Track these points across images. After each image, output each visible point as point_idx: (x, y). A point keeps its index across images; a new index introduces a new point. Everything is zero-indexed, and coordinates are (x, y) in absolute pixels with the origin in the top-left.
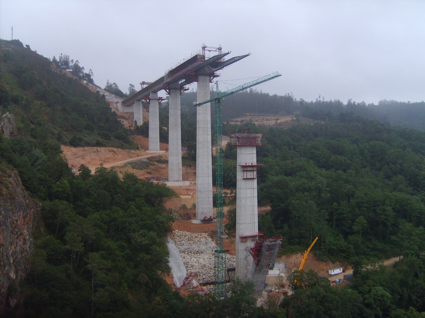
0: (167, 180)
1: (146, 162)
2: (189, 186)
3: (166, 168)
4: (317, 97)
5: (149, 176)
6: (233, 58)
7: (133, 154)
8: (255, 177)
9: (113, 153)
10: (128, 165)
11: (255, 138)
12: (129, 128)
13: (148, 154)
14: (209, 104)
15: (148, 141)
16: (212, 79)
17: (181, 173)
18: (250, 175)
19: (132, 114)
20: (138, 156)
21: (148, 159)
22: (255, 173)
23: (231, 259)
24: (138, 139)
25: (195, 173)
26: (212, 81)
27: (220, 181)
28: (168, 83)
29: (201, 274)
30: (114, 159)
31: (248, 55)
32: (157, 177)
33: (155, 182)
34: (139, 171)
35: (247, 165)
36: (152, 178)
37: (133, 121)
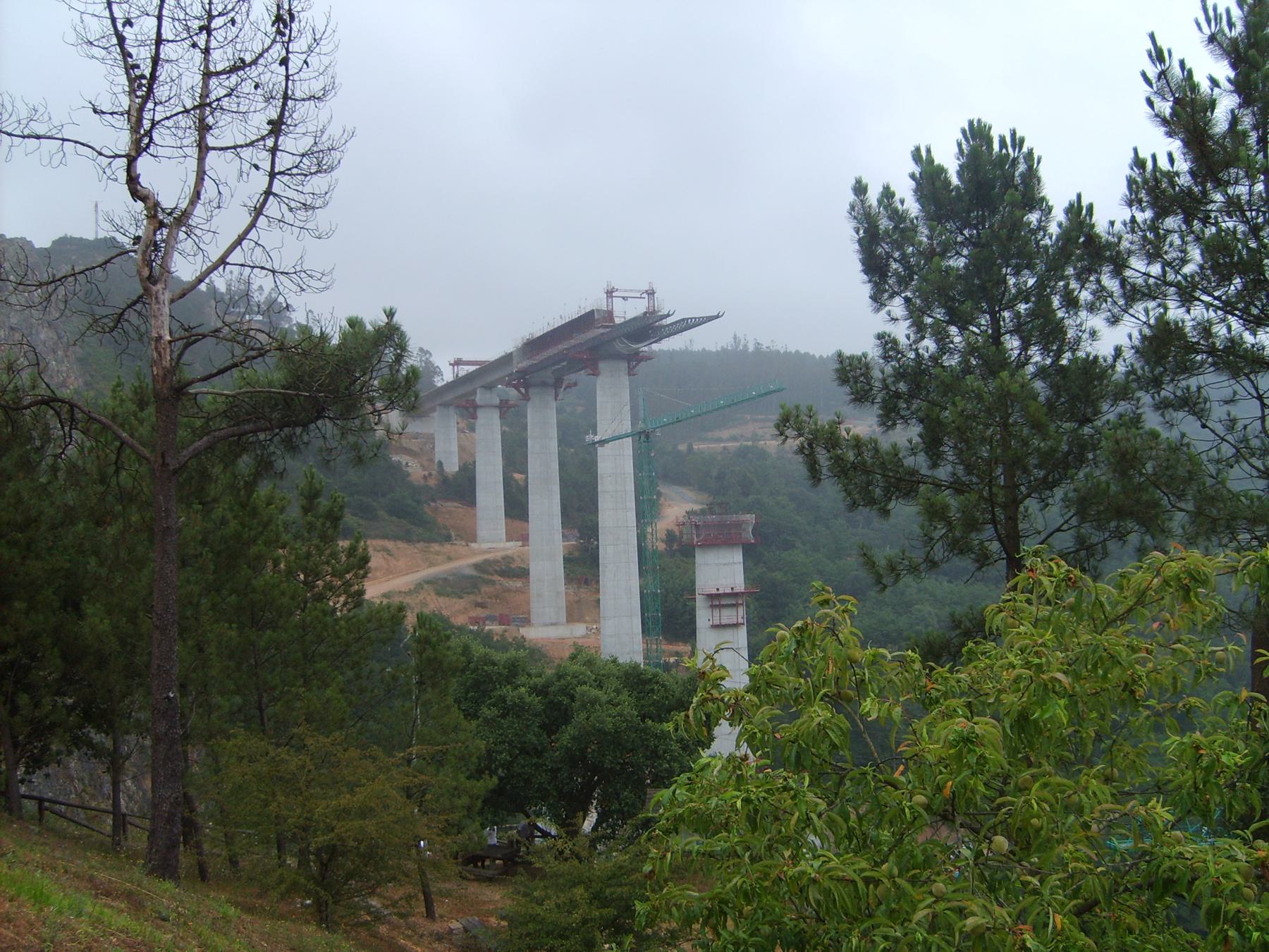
0: (527, 621)
1: (471, 577)
2: (584, 637)
3: (524, 591)
5: (480, 612)
6: (683, 320)
7: (437, 553)
8: (740, 621)
9: (385, 554)
10: (426, 586)
11: (739, 525)
12: (422, 482)
13: (474, 553)
14: (630, 439)
15: (475, 515)
16: (634, 367)
17: (563, 603)
18: (728, 616)
19: (430, 439)
20: (450, 559)
21: (476, 566)
22: (741, 611)
24: (449, 510)
25: (598, 601)
28: (523, 373)
30: (387, 570)
31: (717, 317)
32: (501, 615)
33: (496, 628)
34: (454, 600)
35: (721, 591)
36: (488, 618)
37: (432, 460)
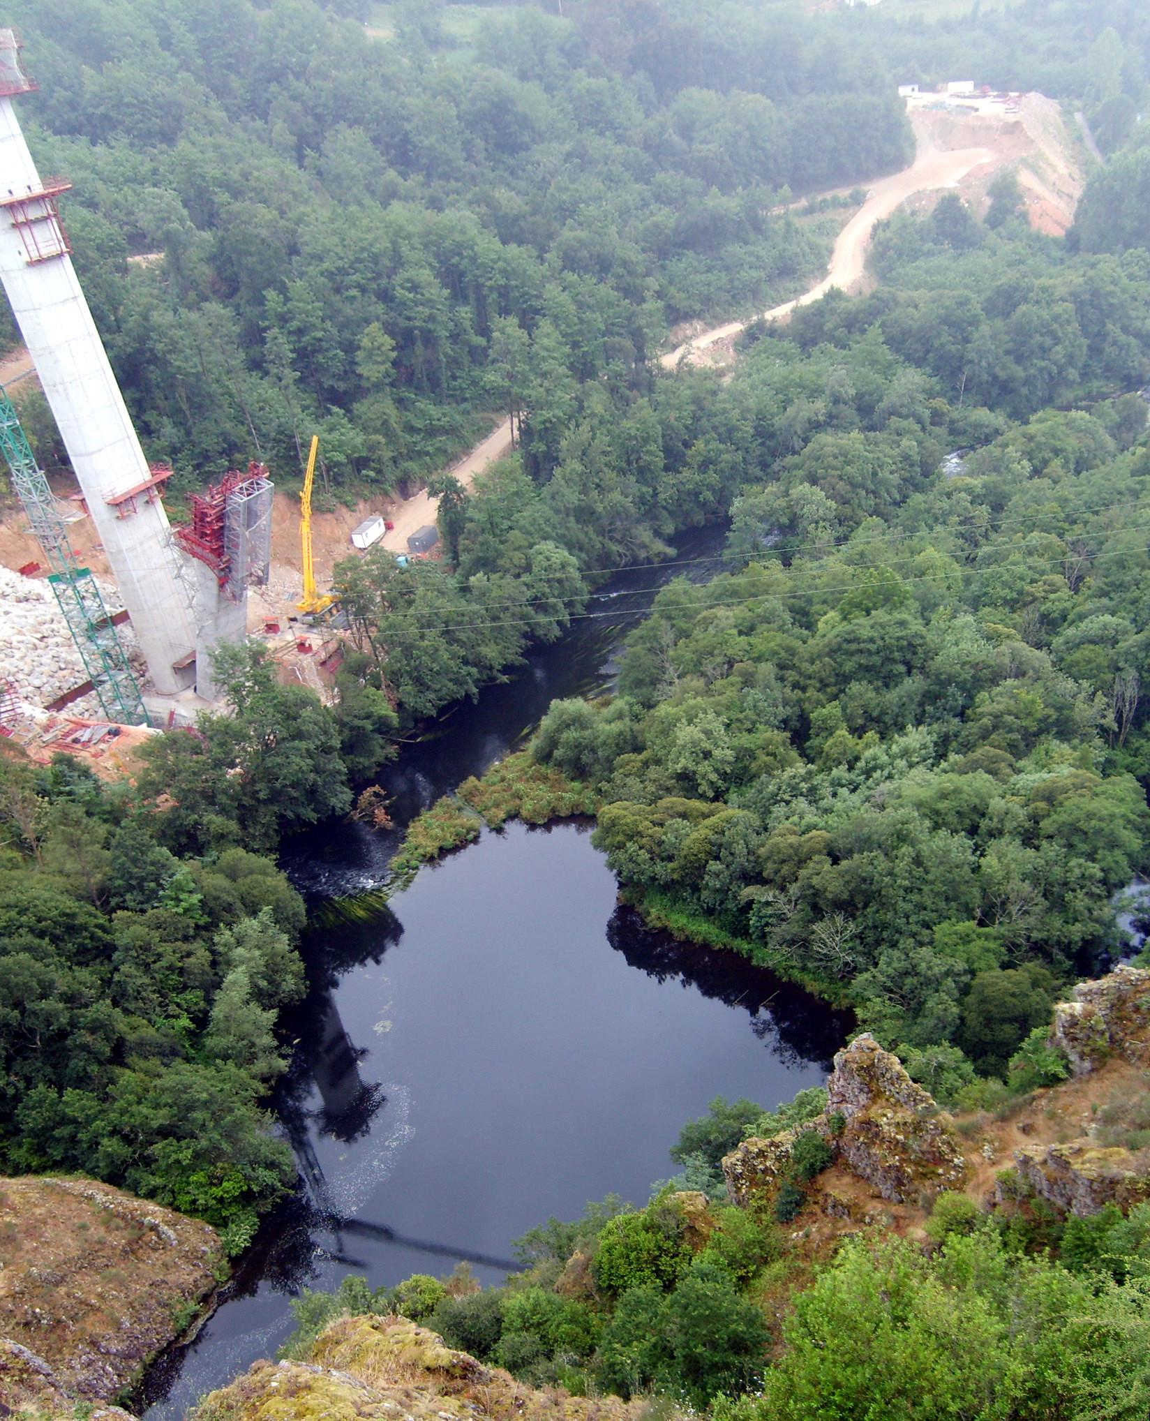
29: (20, 676)
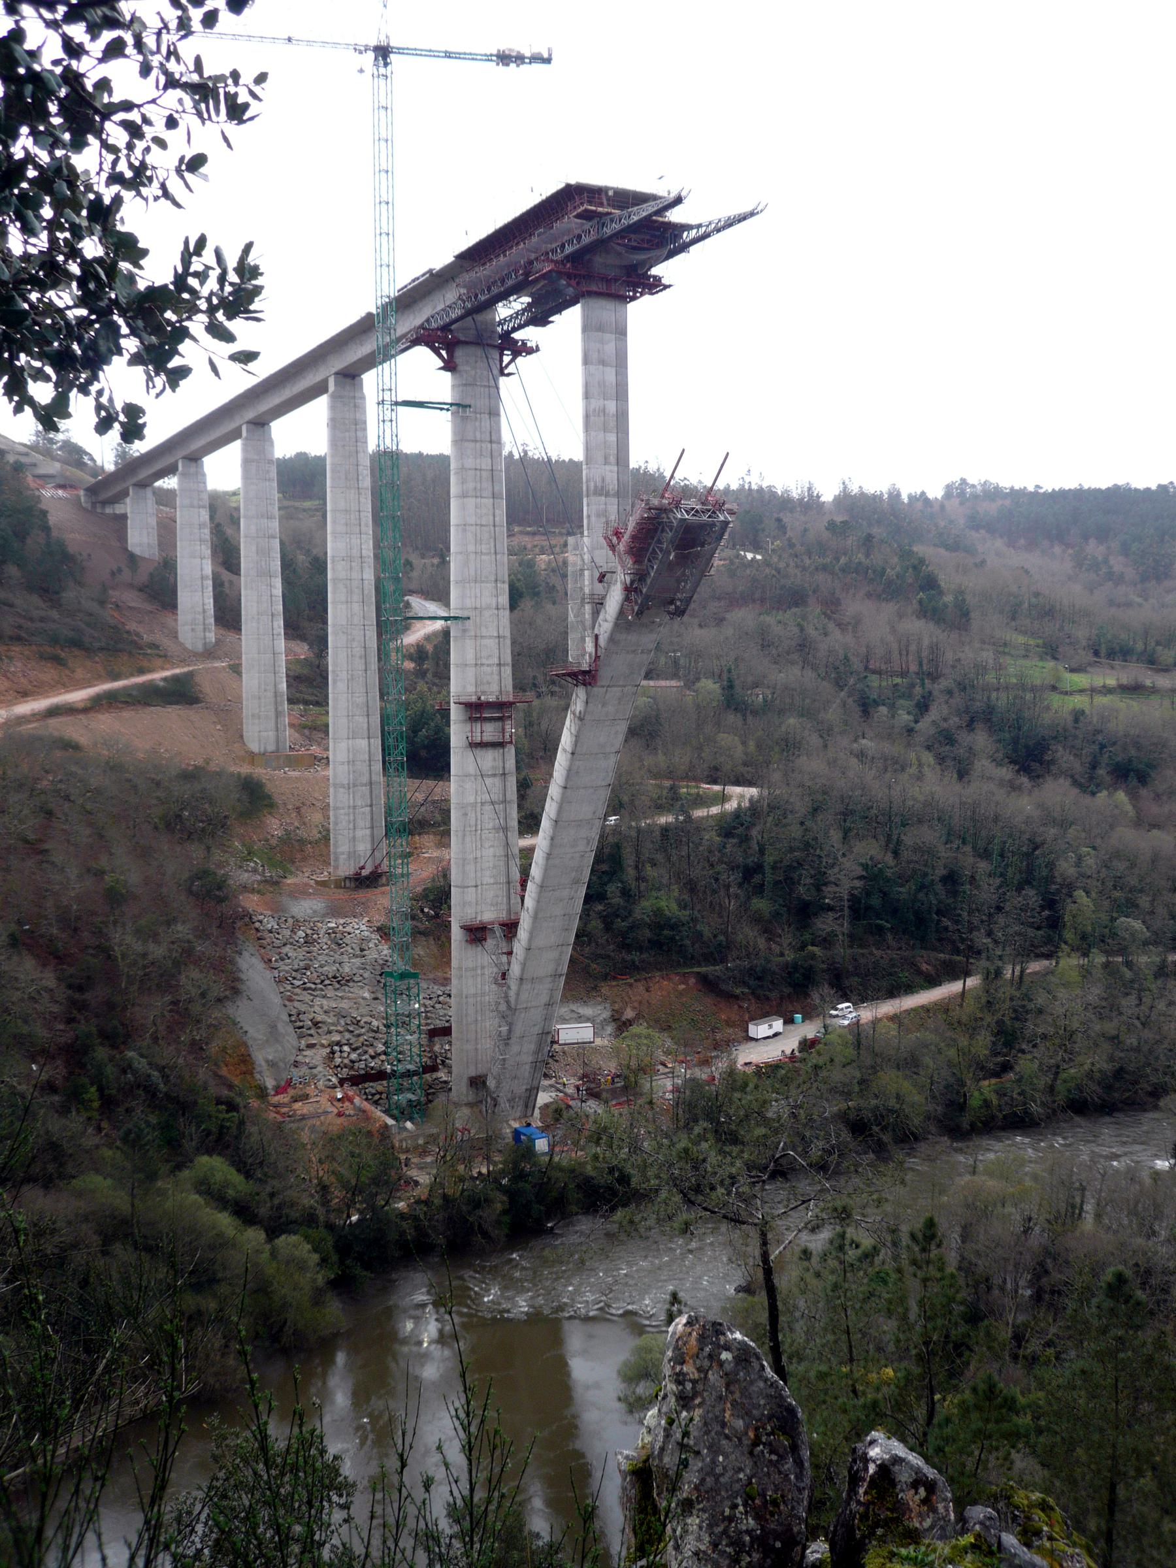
4: (743, 474)
23: (441, 999)
26: (506, 372)
27: (400, 755)
31: (752, 214)
